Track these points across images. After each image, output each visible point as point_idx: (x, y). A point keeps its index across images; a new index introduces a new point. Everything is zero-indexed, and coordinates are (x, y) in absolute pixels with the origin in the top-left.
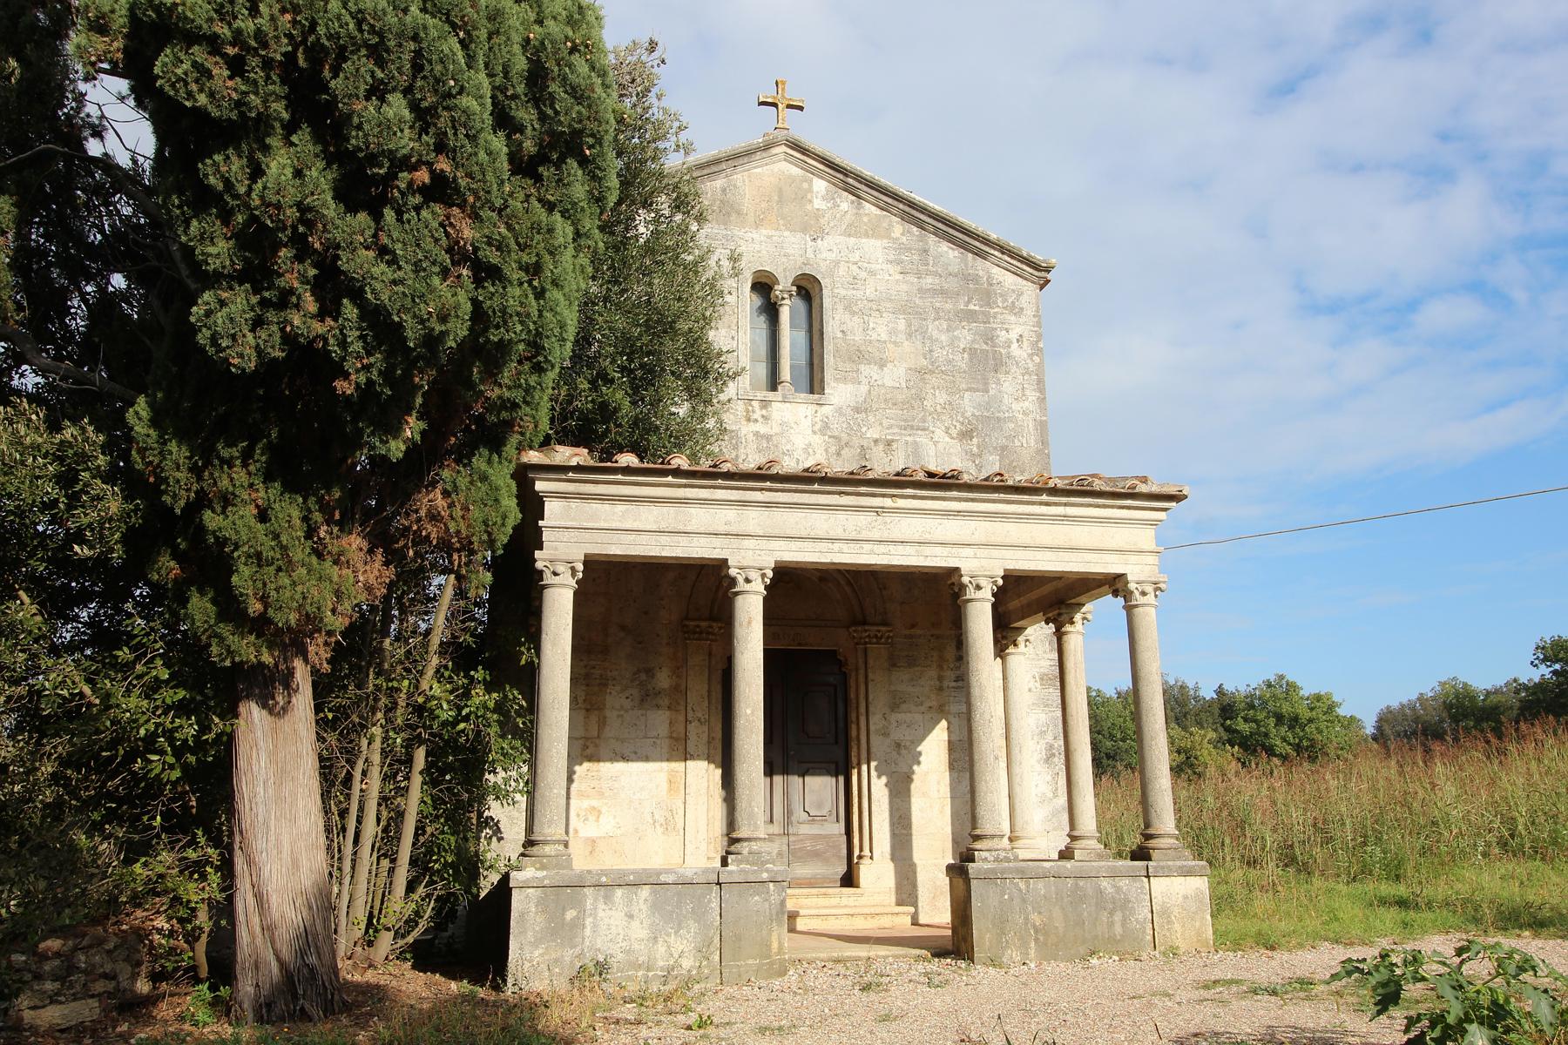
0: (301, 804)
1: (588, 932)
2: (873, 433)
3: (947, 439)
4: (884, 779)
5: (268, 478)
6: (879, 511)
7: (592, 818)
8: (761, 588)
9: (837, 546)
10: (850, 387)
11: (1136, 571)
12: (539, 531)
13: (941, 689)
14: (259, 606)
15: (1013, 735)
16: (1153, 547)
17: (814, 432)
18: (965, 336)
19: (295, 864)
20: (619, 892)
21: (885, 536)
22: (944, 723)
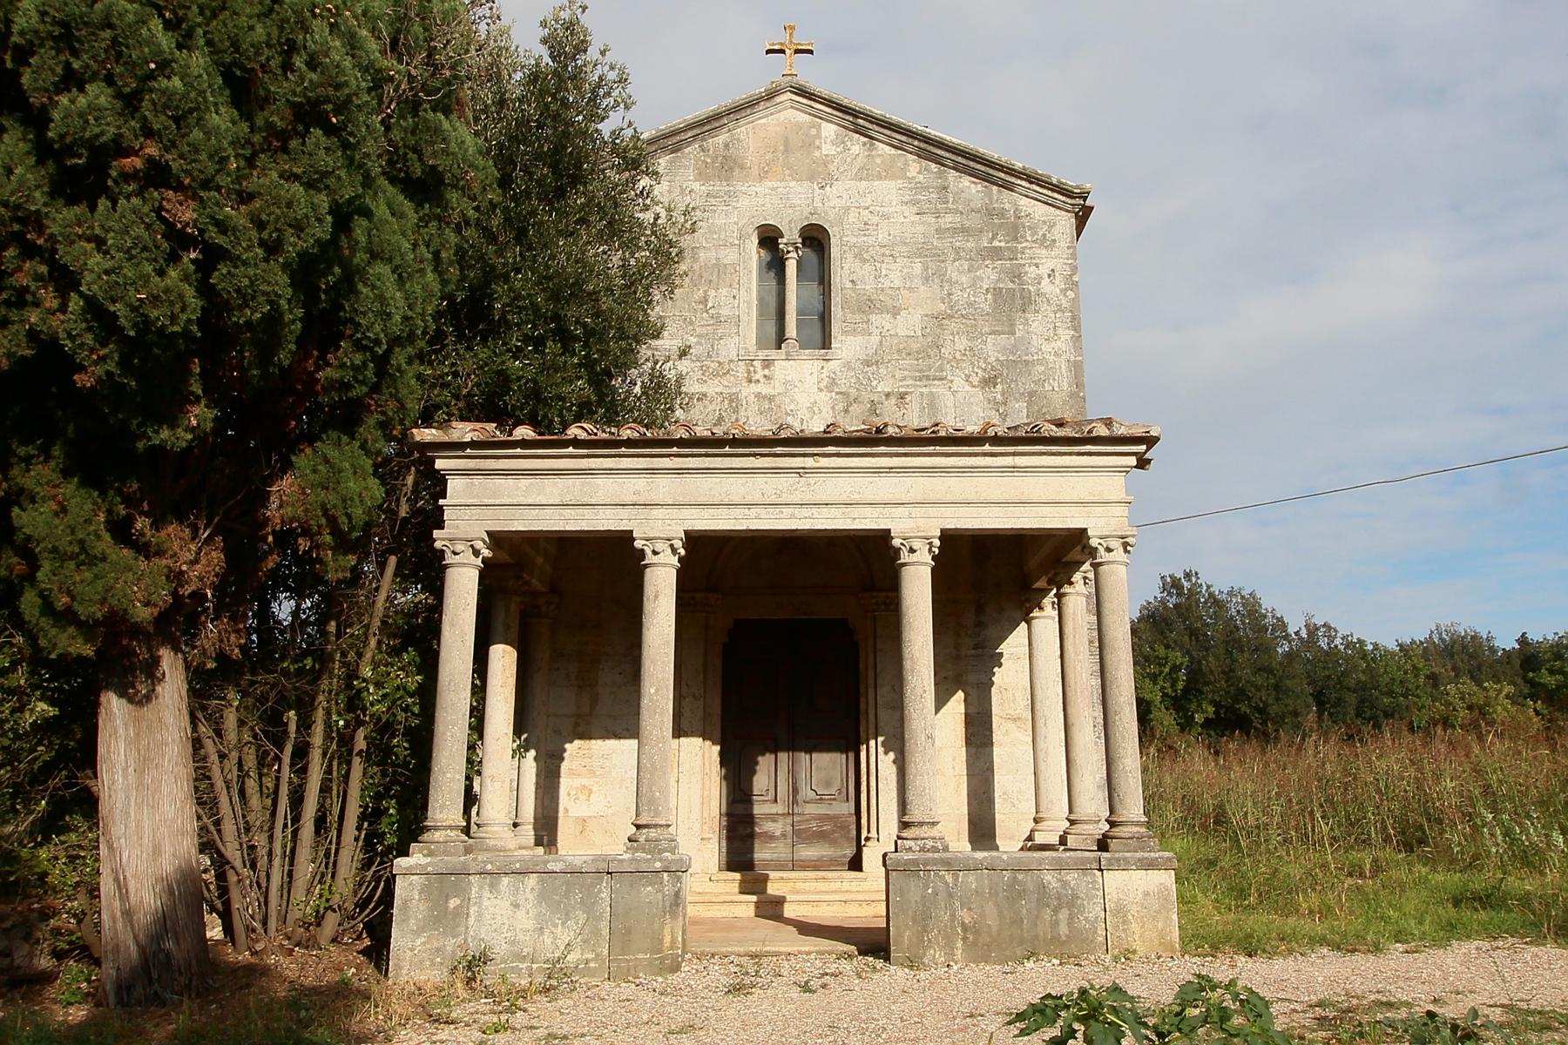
0: (165, 790)
1: (472, 920)
2: (884, 387)
3: (968, 388)
4: (892, 755)
5: (66, 473)
6: (801, 472)
7: (582, 797)
8: (675, 560)
9: (754, 511)
10: (860, 338)
11: (1099, 525)
12: (441, 509)
13: (958, 658)
14: (65, 599)
15: (1038, 706)
16: (1122, 496)
17: (820, 390)
18: (989, 274)
19: (157, 850)
20: (505, 880)
21: (808, 498)
22: (960, 695)
